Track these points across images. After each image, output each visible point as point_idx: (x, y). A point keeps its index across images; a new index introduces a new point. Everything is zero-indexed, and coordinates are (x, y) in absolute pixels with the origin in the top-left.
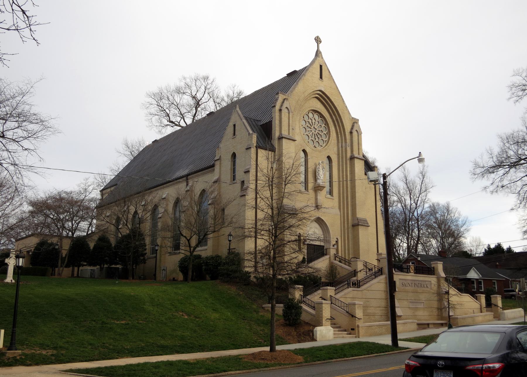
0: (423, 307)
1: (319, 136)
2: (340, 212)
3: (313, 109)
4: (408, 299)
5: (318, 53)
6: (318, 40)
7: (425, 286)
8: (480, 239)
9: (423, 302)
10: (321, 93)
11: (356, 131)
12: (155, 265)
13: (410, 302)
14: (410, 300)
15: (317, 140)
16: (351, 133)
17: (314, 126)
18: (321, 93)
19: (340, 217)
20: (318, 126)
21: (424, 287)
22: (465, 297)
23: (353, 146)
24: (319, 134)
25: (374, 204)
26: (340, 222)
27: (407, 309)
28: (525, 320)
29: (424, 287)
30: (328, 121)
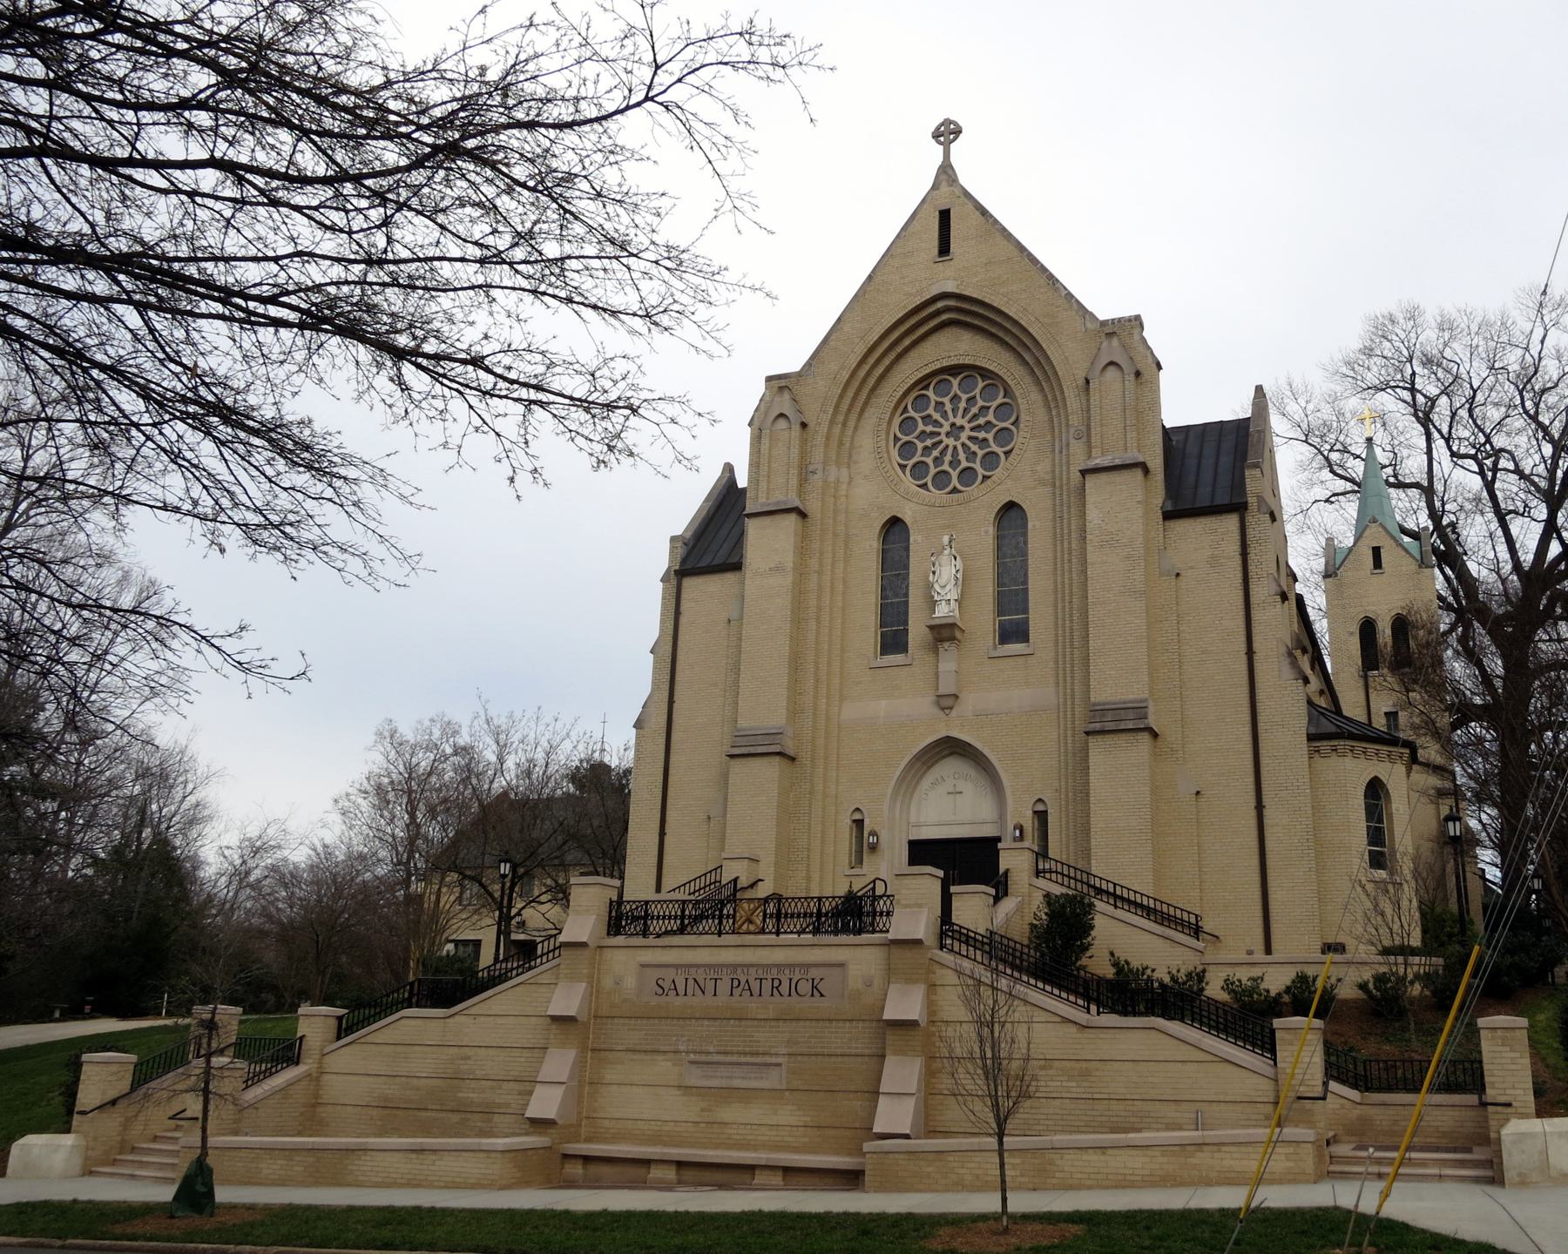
3: (915, 379)
4: (682, 1048)
5: (946, 172)
7: (805, 987)
8: (210, 817)
9: (779, 1065)
10: (952, 303)
13: (692, 1062)
14: (695, 1052)
17: (943, 437)
18: (952, 303)
21: (794, 989)
22: (1121, 1035)
29: (794, 989)
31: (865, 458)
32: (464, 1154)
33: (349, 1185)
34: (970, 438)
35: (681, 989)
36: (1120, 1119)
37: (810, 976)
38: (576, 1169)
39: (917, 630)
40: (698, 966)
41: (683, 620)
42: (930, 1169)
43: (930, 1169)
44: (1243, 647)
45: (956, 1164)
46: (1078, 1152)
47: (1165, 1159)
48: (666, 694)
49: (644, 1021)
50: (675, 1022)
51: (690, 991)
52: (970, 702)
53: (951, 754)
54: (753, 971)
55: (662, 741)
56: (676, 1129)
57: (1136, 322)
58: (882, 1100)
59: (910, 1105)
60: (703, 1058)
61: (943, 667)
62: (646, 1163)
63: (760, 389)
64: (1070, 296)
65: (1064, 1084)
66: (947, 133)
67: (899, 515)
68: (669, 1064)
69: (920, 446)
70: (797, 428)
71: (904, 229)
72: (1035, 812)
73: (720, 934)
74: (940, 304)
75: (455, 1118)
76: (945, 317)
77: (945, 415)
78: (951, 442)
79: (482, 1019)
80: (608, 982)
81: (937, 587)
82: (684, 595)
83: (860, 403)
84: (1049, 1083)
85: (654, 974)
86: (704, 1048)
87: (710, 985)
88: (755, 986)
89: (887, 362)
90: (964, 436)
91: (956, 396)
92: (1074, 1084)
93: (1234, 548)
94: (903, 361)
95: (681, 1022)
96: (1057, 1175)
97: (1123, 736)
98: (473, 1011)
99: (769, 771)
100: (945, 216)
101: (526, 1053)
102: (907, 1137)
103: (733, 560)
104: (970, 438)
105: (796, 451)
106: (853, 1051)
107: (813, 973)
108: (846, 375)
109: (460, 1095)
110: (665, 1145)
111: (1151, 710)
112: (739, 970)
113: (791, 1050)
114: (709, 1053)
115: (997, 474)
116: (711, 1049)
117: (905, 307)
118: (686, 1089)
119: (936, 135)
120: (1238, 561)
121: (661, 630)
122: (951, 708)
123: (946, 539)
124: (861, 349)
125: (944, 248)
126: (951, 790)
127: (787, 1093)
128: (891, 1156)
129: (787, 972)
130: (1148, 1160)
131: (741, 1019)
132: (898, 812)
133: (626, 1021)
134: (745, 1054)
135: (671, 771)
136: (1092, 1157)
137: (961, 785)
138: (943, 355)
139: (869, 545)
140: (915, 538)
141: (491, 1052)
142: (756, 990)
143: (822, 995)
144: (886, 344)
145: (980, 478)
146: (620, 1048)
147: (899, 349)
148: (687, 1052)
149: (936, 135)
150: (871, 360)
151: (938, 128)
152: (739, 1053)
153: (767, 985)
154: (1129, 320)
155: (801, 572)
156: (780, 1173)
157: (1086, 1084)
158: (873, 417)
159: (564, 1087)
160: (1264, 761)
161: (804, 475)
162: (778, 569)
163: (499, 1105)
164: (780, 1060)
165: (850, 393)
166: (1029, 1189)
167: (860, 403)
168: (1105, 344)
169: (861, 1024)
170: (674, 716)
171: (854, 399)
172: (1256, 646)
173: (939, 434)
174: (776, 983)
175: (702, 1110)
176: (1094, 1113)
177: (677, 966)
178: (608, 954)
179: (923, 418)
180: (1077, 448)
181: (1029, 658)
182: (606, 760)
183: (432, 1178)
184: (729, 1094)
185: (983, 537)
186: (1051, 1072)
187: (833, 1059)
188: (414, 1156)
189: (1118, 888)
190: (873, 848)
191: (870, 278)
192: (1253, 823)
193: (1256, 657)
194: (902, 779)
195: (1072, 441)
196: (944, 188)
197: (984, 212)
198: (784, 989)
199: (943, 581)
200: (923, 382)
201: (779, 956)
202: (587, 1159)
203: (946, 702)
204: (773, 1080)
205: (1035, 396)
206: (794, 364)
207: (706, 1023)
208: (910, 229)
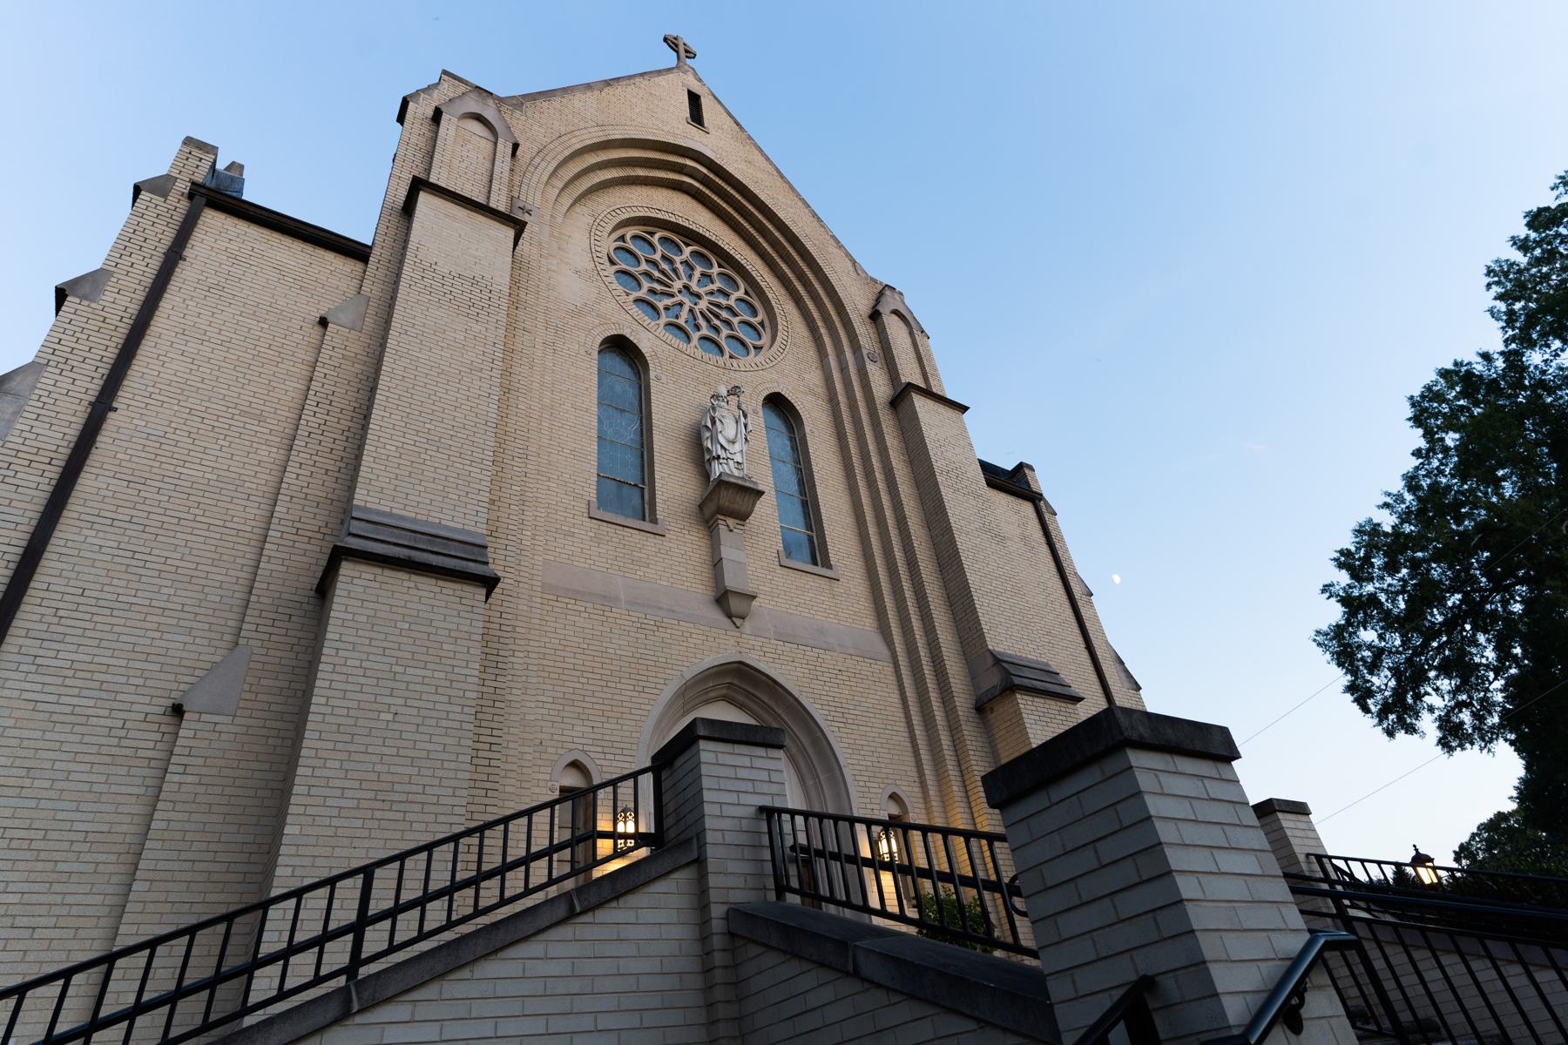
1: (724, 314)
2: (889, 643)
8: (1370, 520)
11: (895, 317)
12: (640, 506)
15: (725, 331)
16: (875, 316)
19: (890, 669)
23: (892, 358)
24: (718, 306)
26: (895, 698)
30: (759, 279)
70: (504, 148)
122: (743, 618)
124: (596, 136)
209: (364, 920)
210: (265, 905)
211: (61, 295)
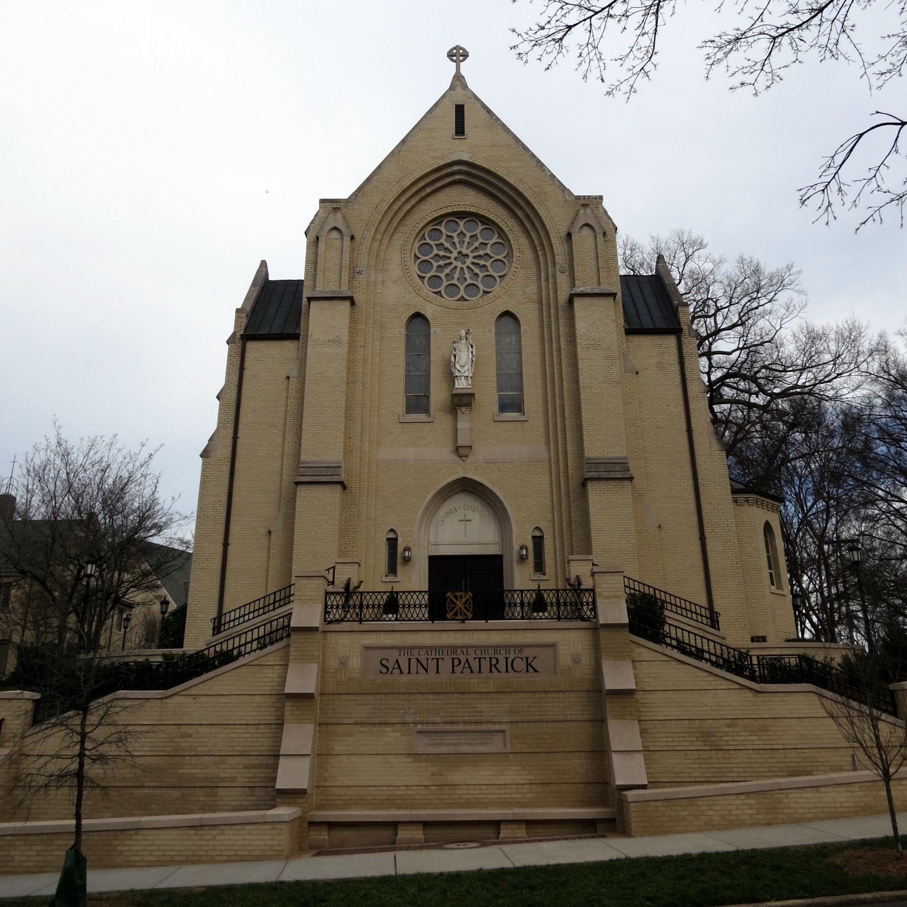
0: (500, 748)
4: (409, 719)
5: (459, 79)
6: (458, 55)
7: (520, 665)
9: (503, 731)
10: (464, 168)
13: (419, 732)
14: (422, 723)
18: (464, 168)
20: (466, 244)
21: (510, 666)
22: (777, 698)
25: (681, 409)
27: (404, 759)
28: (895, 828)
31: (394, 270)
32: (247, 827)
33: (120, 866)
34: (473, 263)
35: (405, 668)
36: (795, 765)
37: (524, 655)
38: (322, 836)
39: (438, 395)
40: (420, 648)
41: (247, 374)
42: (685, 813)
43: (685, 813)
44: (684, 426)
45: (705, 808)
46: (798, 791)
47: (862, 794)
48: (231, 431)
49: (371, 697)
50: (401, 697)
51: (413, 670)
52: (481, 452)
53: (461, 491)
54: (472, 651)
55: (226, 469)
56: (408, 792)
57: (601, 198)
58: (282, 762)
59: (305, 763)
60: (430, 728)
61: (460, 425)
62: (394, 825)
63: (316, 207)
64: (552, 176)
65: (748, 738)
66: (458, 55)
67: (422, 312)
68: (398, 734)
69: (435, 264)
70: (347, 239)
71: (430, 112)
72: (533, 537)
73: (361, 621)
74: (456, 168)
75: (176, 793)
76: (457, 177)
77: (462, 243)
78: (459, 264)
79: (203, 699)
80: (333, 663)
81: (458, 366)
82: (247, 355)
83: (392, 229)
84: (736, 738)
85: (379, 655)
86: (431, 719)
87: (432, 665)
88: (475, 665)
89: (413, 202)
90: (469, 261)
91: (462, 232)
92: (756, 738)
93: (673, 358)
94: (423, 203)
95: (407, 697)
96: (786, 811)
97: (612, 483)
98: (194, 691)
99: (332, 495)
100: (460, 110)
101: (252, 730)
102: (644, 787)
103: (291, 331)
104: (473, 263)
105: (348, 256)
106: (569, 718)
107: (527, 652)
108: (385, 206)
109: (181, 771)
110: (399, 807)
111: (631, 465)
112: (459, 651)
113: (513, 719)
114: (435, 723)
115: (497, 289)
116: (438, 720)
117: (430, 165)
118: (415, 756)
119: (450, 55)
120: (676, 368)
121: (227, 380)
122: (467, 456)
123: (463, 333)
124: (397, 190)
125: (460, 130)
126: (463, 518)
127: (511, 756)
128: (652, 804)
129: (503, 652)
130: (850, 794)
131: (463, 693)
132: (422, 533)
133: (353, 697)
134: (470, 723)
135: (235, 493)
136: (808, 794)
137: (470, 515)
138: (454, 203)
139: (397, 332)
140: (435, 330)
141: (215, 729)
142: (475, 666)
143: (536, 671)
144: (414, 189)
145: (459, 296)
146: (348, 721)
147: (423, 194)
148: (415, 723)
149: (450, 55)
150: (403, 199)
151: (451, 50)
152: (465, 723)
153: (485, 664)
154: (596, 198)
155: (352, 346)
156: (523, 826)
157: (764, 738)
158: (398, 240)
159: (308, 759)
160: (704, 506)
161: (354, 273)
162: (336, 341)
163: (225, 779)
164: (503, 727)
165: (387, 220)
166: (765, 825)
167: (392, 229)
168: (582, 211)
169: (573, 695)
170: (238, 449)
171: (389, 224)
172: (693, 426)
173: (449, 258)
174: (494, 662)
175: (433, 774)
176: (775, 760)
177: (400, 648)
178: (332, 638)
179: (436, 245)
180: (563, 281)
181: (525, 424)
182: (13, 493)
183: (212, 853)
184: (458, 759)
185: (487, 333)
186: (736, 729)
187: (551, 725)
188: (192, 832)
189: (657, 592)
190: (407, 560)
191: (403, 141)
192: (697, 548)
193: (694, 434)
194: (427, 508)
195: (558, 273)
196: (459, 90)
197: (489, 111)
198: (502, 665)
199: (463, 362)
200: (438, 220)
201: (496, 638)
202: (331, 825)
203: (462, 451)
204: (495, 745)
205: (523, 240)
206: (344, 193)
207: (431, 697)
208: (434, 113)
209: (275, 602)
210: (290, 586)
211: (218, 397)
